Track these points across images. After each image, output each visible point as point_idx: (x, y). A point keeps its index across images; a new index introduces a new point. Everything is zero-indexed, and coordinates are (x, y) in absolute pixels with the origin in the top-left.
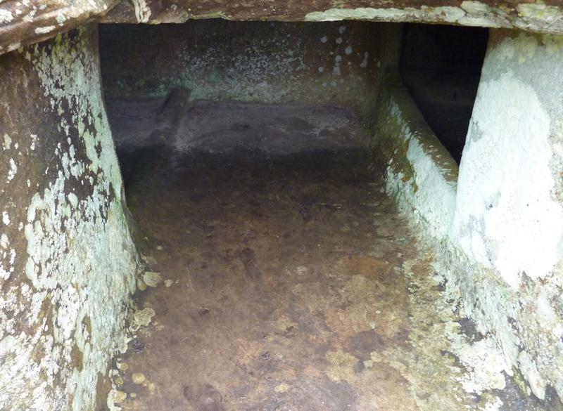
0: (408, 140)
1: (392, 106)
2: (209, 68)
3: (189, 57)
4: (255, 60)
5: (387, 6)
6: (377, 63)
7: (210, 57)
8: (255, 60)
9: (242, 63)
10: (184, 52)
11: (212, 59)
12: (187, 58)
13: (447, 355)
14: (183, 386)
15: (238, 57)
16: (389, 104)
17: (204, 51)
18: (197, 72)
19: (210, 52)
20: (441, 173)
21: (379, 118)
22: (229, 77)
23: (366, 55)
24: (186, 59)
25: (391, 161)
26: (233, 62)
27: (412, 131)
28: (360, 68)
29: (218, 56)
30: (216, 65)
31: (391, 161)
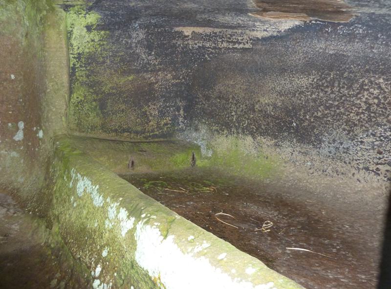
0: (131, 233)
1: (77, 181)
5: (365, 2)
6: (37, 132)
16: (69, 178)
20: (80, 16)
21: (55, 201)
23: (21, 125)
25: (99, 269)
27: (135, 212)
28: (14, 141)
31: (99, 269)
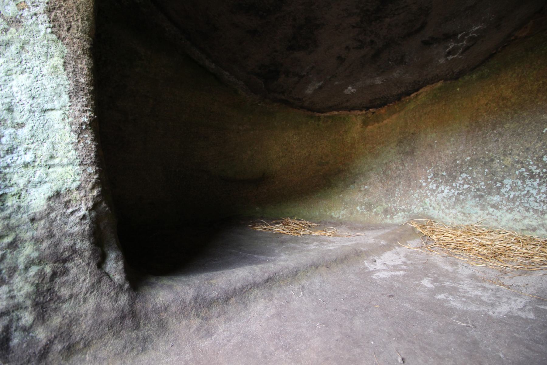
2: (462, 197)
3: (435, 185)
4: (535, 183)
7: (463, 185)
8: (535, 183)
9: (512, 189)
10: (429, 180)
11: (466, 186)
12: (433, 186)
13: (37, 261)
14: (102, 269)
15: (505, 181)
17: (455, 178)
18: (445, 200)
19: (463, 179)
22: (493, 206)
24: (430, 187)
26: (499, 188)
29: (475, 183)
30: (473, 194)
